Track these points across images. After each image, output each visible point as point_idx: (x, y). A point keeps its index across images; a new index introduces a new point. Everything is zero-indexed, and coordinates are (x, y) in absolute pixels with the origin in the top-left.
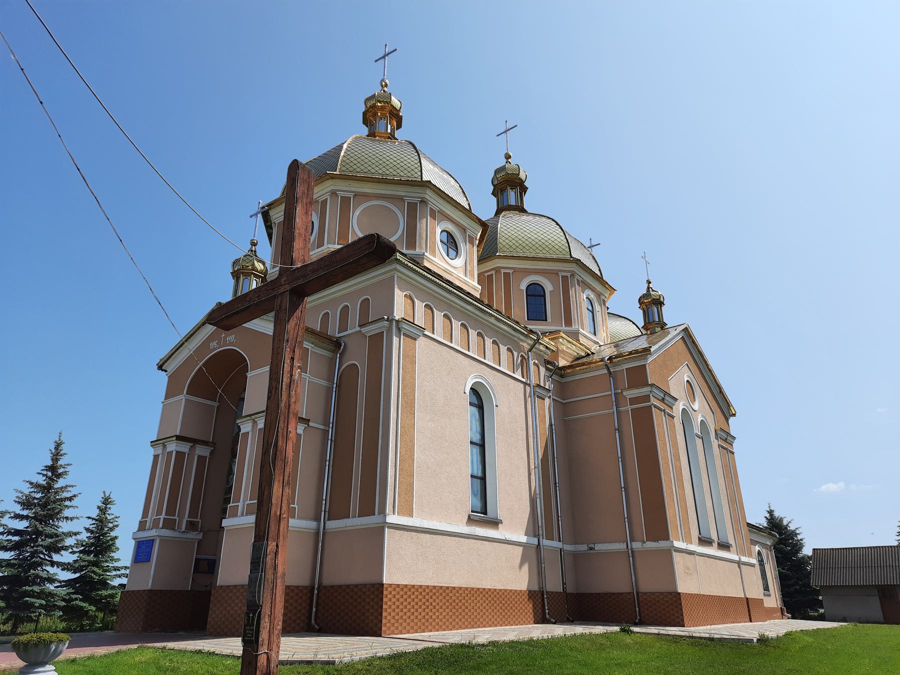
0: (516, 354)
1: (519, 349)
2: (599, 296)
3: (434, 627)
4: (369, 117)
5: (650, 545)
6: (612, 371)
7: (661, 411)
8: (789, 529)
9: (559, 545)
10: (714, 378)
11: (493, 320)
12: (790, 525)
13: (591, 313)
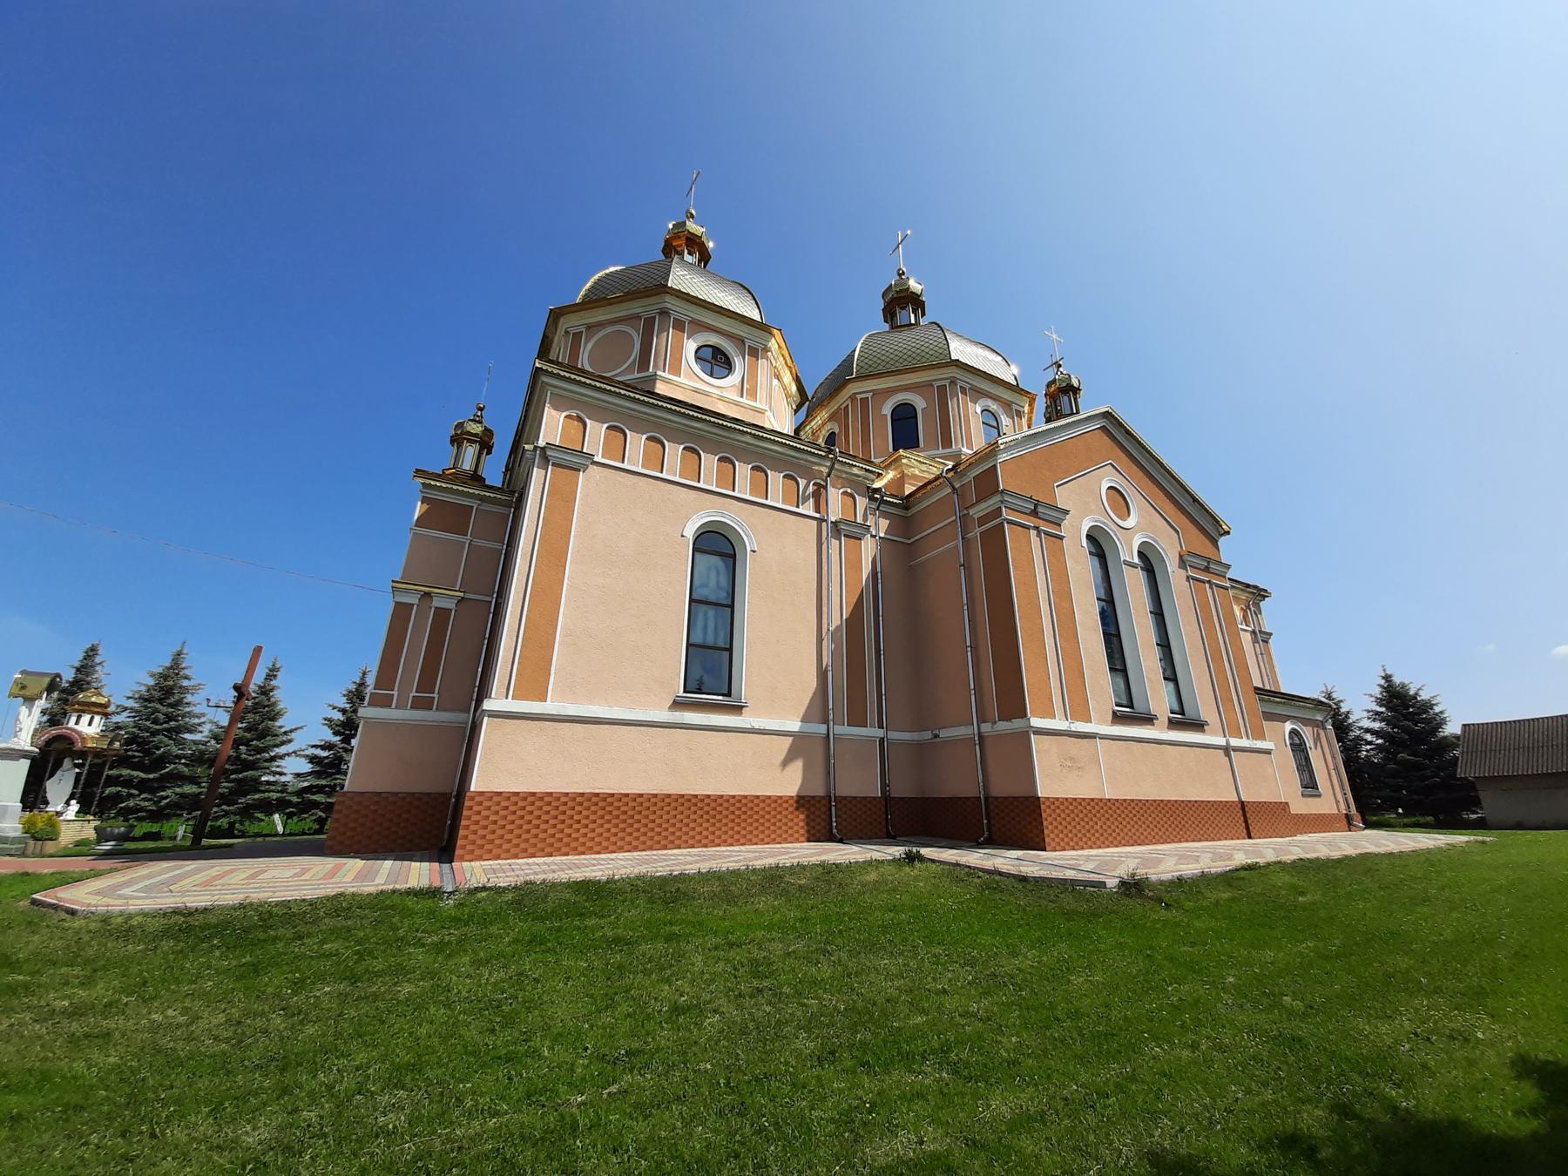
0: (802, 483)
1: (809, 474)
2: (1009, 405)
3: (1112, 842)
4: (889, 313)
5: (1003, 726)
6: (957, 486)
7: (1029, 529)
8: (1419, 699)
9: (880, 733)
10: (1176, 479)
11: (748, 439)
12: (1421, 693)
13: (996, 431)
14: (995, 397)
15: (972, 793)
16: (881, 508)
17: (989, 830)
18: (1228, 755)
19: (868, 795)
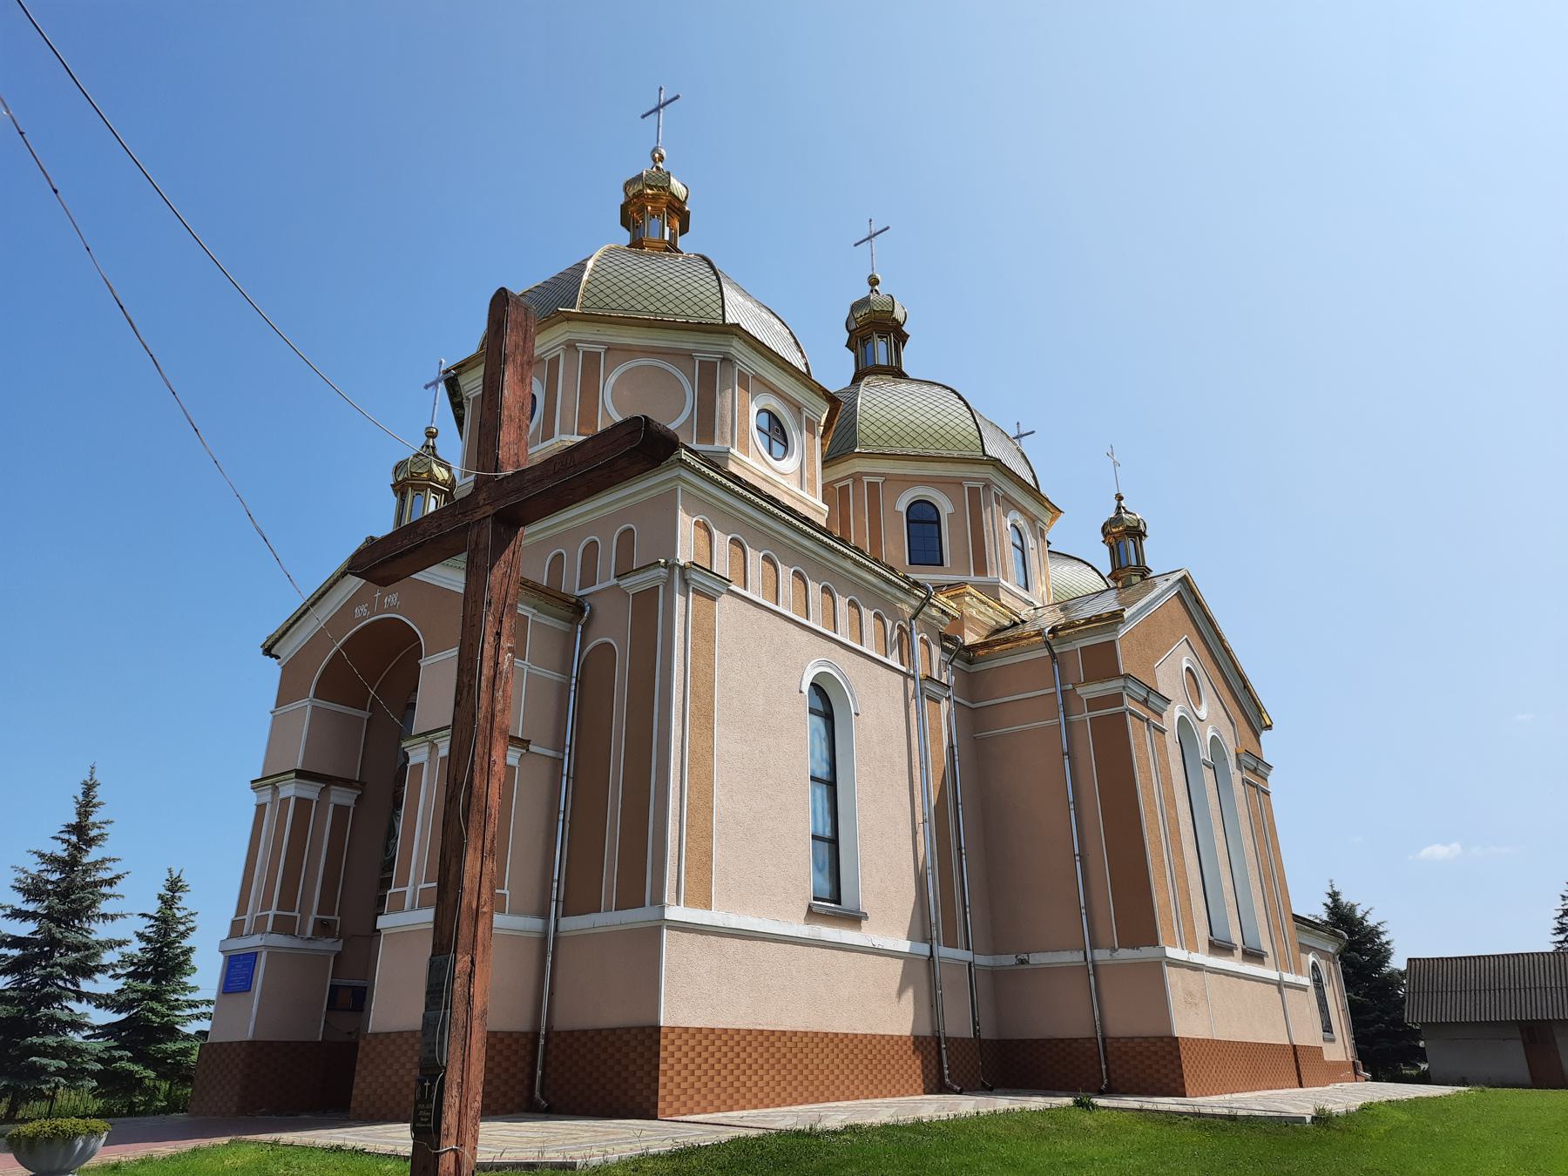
0: (889, 623)
1: (896, 614)
4: (632, 215)
5: (1125, 954)
6: (1056, 651)
8: (1365, 924)
9: (967, 956)
11: (848, 565)
13: (1019, 552)
14: (783, 394)
15: (1088, 1034)
16: (954, 663)
17: (1108, 1077)
18: (1280, 992)
19: (234, 1040)
